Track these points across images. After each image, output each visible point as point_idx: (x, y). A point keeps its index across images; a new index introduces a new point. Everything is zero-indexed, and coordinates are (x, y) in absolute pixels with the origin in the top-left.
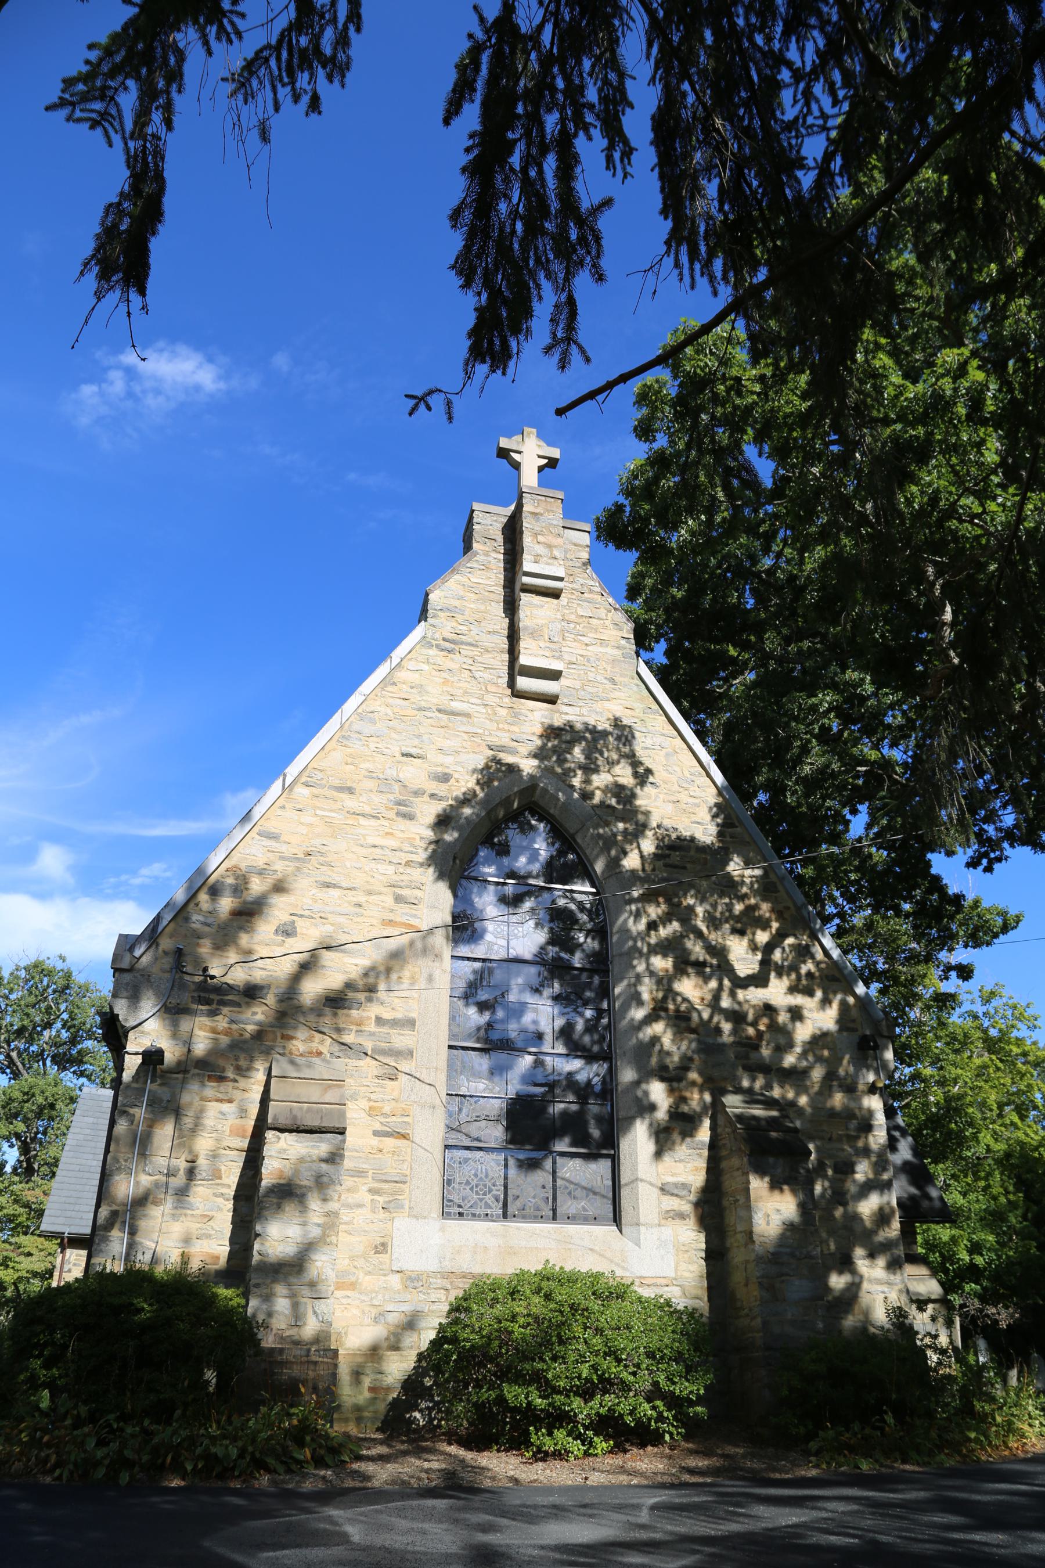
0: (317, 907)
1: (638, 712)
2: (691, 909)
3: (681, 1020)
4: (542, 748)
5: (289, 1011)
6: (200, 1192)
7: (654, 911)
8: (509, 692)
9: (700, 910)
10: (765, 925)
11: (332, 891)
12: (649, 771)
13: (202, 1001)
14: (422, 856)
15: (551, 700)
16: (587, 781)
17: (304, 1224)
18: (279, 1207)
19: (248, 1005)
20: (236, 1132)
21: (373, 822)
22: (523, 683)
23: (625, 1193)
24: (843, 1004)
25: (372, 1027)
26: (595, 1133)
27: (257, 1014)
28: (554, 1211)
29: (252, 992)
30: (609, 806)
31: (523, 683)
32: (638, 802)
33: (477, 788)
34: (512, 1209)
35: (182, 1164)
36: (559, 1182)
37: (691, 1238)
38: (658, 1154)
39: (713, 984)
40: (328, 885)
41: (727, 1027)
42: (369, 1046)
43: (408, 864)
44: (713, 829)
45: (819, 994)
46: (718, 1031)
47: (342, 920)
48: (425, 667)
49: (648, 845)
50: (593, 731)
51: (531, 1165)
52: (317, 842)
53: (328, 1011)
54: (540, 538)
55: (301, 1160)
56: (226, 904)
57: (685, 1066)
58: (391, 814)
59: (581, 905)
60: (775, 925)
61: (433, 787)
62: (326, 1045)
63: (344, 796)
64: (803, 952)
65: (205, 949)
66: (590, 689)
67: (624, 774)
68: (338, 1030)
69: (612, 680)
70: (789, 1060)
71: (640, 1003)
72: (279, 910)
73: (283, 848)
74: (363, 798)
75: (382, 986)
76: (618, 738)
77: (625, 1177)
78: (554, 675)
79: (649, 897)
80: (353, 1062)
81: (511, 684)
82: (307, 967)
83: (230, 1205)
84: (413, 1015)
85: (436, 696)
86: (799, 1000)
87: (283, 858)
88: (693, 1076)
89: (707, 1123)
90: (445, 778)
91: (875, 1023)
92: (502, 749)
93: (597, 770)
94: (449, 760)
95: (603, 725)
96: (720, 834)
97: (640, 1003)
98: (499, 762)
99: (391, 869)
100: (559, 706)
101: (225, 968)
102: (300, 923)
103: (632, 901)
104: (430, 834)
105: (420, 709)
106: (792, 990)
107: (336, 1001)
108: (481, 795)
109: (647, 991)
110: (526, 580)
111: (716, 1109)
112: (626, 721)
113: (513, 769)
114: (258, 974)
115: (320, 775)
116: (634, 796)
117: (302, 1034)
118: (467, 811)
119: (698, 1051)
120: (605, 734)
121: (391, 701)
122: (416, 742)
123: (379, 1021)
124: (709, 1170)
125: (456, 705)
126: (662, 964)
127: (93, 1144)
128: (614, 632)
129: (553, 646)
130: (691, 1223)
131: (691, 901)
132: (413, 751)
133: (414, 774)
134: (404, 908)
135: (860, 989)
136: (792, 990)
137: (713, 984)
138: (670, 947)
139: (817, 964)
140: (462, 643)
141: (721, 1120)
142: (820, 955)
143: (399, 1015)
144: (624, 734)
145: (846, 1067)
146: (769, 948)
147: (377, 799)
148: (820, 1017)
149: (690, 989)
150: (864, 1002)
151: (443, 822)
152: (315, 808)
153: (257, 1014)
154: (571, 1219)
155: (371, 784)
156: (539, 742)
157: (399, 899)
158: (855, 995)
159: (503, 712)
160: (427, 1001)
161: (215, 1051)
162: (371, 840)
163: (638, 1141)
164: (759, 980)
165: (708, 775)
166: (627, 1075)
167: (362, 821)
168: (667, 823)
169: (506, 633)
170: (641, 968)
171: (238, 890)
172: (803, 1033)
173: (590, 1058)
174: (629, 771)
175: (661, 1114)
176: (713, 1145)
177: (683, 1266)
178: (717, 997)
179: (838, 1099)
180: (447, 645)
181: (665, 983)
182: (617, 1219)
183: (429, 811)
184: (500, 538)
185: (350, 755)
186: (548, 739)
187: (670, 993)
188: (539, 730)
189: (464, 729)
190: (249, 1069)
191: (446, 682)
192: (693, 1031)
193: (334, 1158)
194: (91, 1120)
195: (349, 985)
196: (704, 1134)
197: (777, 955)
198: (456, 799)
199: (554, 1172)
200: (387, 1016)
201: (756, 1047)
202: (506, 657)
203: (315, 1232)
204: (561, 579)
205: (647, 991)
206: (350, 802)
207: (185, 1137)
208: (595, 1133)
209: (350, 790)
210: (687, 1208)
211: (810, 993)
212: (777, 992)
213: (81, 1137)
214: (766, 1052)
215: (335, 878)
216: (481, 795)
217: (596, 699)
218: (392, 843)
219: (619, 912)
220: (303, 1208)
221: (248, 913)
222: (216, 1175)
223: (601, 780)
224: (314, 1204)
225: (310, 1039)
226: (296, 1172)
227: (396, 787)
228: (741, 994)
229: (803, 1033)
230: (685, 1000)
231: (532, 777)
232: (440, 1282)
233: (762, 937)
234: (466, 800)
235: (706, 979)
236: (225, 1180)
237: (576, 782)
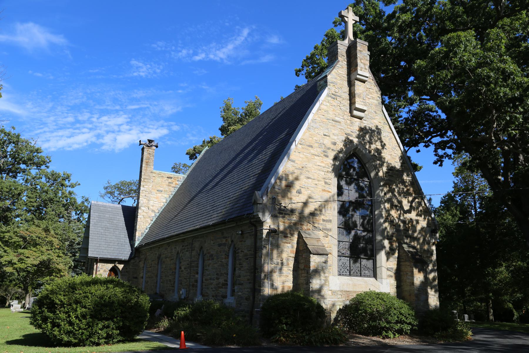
0: (306, 185)
1: (382, 124)
2: (394, 189)
3: (392, 222)
4: (359, 135)
5: (302, 218)
6: (285, 269)
7: (386, 189)
8: (350, 115)
9: (396, 190)
10: (410, 195)
11: (310, 180)
12: (385, 144)
13: (280, 213)
14: (331, 169)
15: (361, 118)
16: (370, 147)
17: (320, 280)
18: (315, 275)
19: (292, 215)
20: (292, 252)
21: (318, 158)
22: (355, 113)
23: (378, 269)
24: (428, 219)
25: (321, 222)
26: (369, 252)
27: (295, 218)
28: (361, 274)
29: (292, 211)
30: (375, 155)
31: (355, 113)
32: (382, 155)
33: (343, 147)
34: (352, 272)
35: (280, 262)
36: (362, 266)
37: (393, 282)
38: (388, 260)
39: (399, 212)
40: (308, 178)
41: (402, 225)
42: (321, 227)
43: (328, 172)
44: (400, 164)
45: (423, 216)
46: (400, 226)
47: (312, 189)
48: (328, 104)
49: (385, 169)
50: (371, 130)
51: (355, 262)
52: (305, 163)
53: (311, 217)
54: (362, 61)
55: (319, 262)
56: (284, 183)
57: (392, 236)
58: (322, 155)
59: (366, 186)
60: (414, 195)
61: (332, 147)
62: (310, 226)
63: (310, 148)
64: (420, 204)
65: (280, 198)
66: (370, 115)
67: (378, 145)
68: (313, 223)
69: (376, 112)
70: (416, 235)
71: (383, 217)
72: (297, 185)
73: (296, 165)
74: (315, 150)
75: (323, 210)
76: (377, 133)
77: (378, 265)
78: (363, 111)
79: (384, 185)
80: (318, 232)
81: (351, 112)
82: (305, 204)
83: (292, 273)
84: (331, 219)
85: (331, 116)
86: (418, 218)
87: (296, 169)
88: (394, 239)
89: (397, 251)
90: (335, 144)
91: (435, 226)
92: (349, 134)
93: (372, 144)
94: (336, 138)
95: (374, 128)
96: (401, 166)
97: (383, 217)
98: (348, 139)
99: (323, 173)
100: (363, 120)
101: (285, 203)
102: (302, 190)
103: (381, 186)
104: (332, 162)
105: (328, 119)
106: (417, 215)
107: (313, 214)
108: (344, 150)
109: (384, 214)
110: (358, 76)
111: (400, 248)
112: (379, 127)
113: (352, 142)
114: (294, 206)
115: (303, 141)
116: (381, 152)
117: (305, 224)
118: (341, 155)
119: (396, 231)
120: (374, 131)
121: (320, 116)
122: (327, 131)
123: (324, 220)
124: (398, 265)
125: (337, 119)
126: (387, 205)
127: (100, 224)
128: (376, 95)
129: (364, 101)
130: (393, 278)
131: (394, 187)
132: (327, 134)
133: (327, 142)
134: (327, 186)
135: (433, 216)
136: (417, 215)
137: (399, 212)
138: (389, 201)
139: (423, 207)
140: (337, 96)
141: (401, 251)
142: (423, 205)
143: (328, 219)
144: (379, 131)
145: (428, 237)
146: (412, 202)
147: (319, 150)
148: (423, 223)
149: (394, 213)
150: (433, 219)
151: (335, 158)
152: (303, 152)
153: (295, 218)
154: (365, 276)
155: (317, 145)
156: (358, 133)
157: (326, 183)
158: (431, 217)
159: (349, 122)
160: (331, 216)
161: (285, 229)
162: (318, 164)
163: (382, 256)
164: (409, 211)
165: (399, 147)
166: (379, 238)
167: (316, 157)
168: (389, 162)
169: (348, 93)
170: (382, 207)
171: (286, 180)
172: (419, 227)
173: (368, 232)
174: (380, 144)
175: (387, 248)
176: (398, 258)
177: (392, 290)
178: (400, 216)
179: (426, 247)
180: (333, 96)
181: (388, 211)
182: (375, 276)
183: (332, 155)
184: (345, 55)
185: (311, 134)
186: (360, 132)
187: (389, 215)
188: (358, 128)
189: (339, 127)
190: (293, 234)
191: (334, 110)
192: (394, 225)
193: (326, 262)
194: (97, 214)
195: (316, 210)
196: (396, 255)
197: (414, 204)
198: (338, 151)
199: (360, 263)
200: (325, 219)
201: (408, 231)
202: (349, 102)
203: (323, 282)
204: (367, 77)
205: (384, 214)
206: (312, 151)
207: (280, 253)
208: (369, 252)
209: (312, 147)
210: (393, 274)
211: (421, 216)
212: (413, 215)
213: (95, 221)
214: (410, 232)
215: (310, 176)
216: (344, 150)
217: (372, 118)
218: (323, 165)
219: (378, 189)
220: (320, 276)
221: (290, 186)
222: (288, 264)
223: (373, 147)
224: (322, 274)
225: (307, 225)
226: (318, 266)
227: (323, 146)
228: (405, 215)
229: (419, 227)
230: (393, 216)
231: (357, 144)
232: (340, 293)
233: (411, 199)
234: (340, 152)
235: (398, 210)
236: (290, 266)
237: (367, 147)
